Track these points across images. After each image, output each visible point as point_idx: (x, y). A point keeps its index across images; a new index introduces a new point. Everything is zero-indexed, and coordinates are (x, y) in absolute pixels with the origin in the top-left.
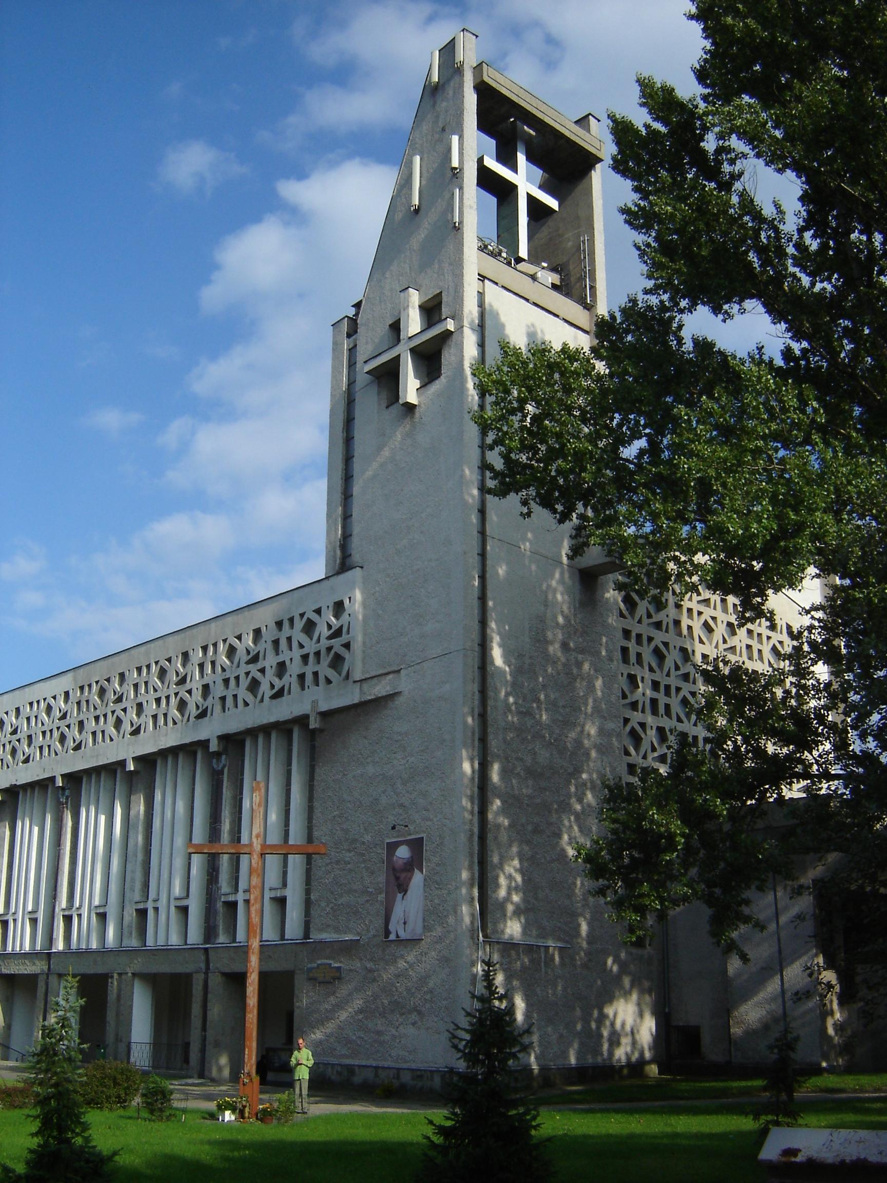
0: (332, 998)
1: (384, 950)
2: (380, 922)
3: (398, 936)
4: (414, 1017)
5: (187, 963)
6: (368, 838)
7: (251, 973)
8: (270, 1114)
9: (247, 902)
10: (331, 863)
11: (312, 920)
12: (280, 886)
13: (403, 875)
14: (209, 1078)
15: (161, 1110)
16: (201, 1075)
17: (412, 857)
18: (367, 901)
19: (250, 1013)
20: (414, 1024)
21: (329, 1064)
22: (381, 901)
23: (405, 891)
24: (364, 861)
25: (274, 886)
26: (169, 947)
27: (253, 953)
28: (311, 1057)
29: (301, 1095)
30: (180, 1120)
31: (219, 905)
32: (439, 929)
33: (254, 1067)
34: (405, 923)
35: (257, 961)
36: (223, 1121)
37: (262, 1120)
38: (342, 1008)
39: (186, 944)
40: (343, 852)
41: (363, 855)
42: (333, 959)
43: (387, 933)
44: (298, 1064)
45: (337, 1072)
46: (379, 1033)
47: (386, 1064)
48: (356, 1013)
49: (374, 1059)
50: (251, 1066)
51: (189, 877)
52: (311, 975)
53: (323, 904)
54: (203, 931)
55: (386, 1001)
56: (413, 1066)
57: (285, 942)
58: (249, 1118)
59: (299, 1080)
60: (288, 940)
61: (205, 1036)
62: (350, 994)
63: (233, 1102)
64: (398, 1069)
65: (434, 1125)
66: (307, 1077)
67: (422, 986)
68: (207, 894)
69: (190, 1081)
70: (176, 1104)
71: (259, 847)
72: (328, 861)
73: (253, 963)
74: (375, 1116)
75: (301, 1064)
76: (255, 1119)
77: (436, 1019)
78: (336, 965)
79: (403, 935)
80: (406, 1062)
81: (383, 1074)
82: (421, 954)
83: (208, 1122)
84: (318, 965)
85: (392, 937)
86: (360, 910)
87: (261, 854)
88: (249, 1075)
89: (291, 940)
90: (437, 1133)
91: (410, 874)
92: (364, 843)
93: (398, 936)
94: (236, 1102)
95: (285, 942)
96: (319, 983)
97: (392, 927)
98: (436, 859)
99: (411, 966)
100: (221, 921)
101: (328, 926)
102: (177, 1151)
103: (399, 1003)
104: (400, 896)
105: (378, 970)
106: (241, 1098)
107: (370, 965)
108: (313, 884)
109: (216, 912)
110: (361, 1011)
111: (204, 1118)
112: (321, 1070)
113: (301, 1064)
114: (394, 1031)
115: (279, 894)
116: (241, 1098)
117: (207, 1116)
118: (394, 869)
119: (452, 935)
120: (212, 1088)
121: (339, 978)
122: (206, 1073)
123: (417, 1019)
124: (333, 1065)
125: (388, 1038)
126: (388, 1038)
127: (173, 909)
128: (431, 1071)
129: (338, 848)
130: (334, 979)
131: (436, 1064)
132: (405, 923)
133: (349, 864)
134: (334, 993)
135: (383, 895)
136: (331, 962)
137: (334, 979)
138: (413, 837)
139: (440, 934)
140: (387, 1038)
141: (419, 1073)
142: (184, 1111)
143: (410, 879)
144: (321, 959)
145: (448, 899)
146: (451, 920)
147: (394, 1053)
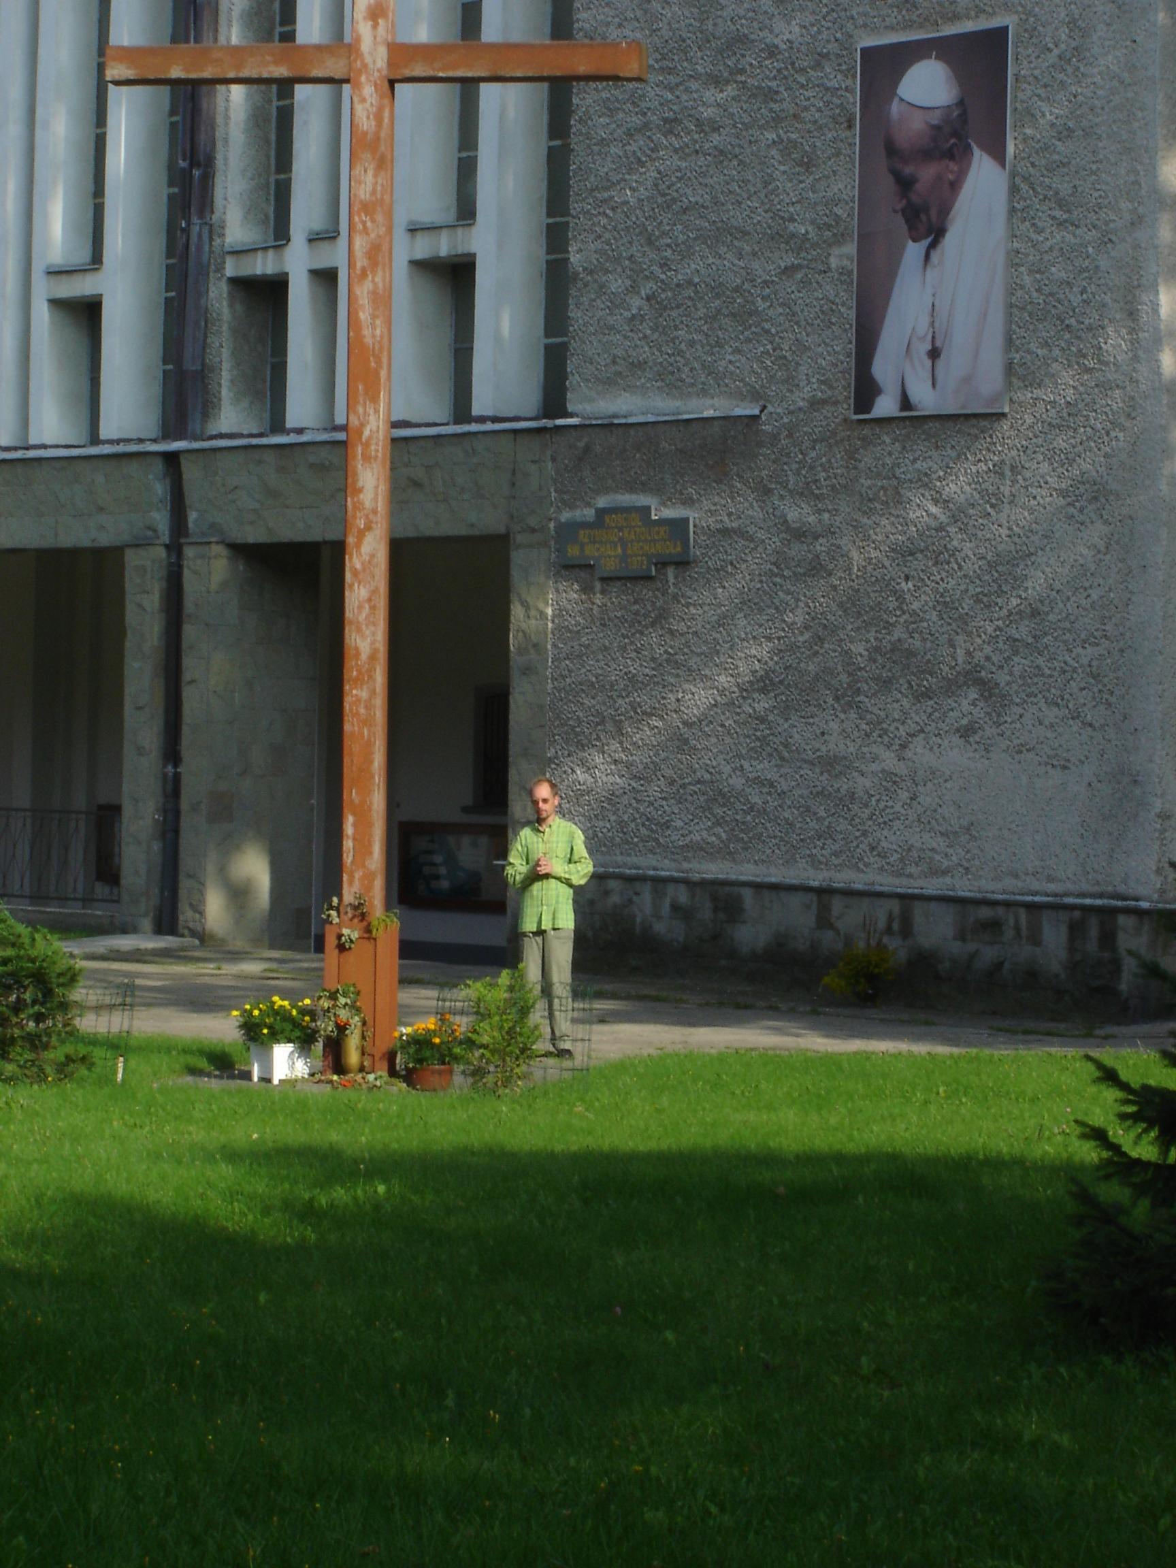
0: (654, 637)
1: (851, 455)
2: (843, 344)
3: (906, 403)
4: (967, 704)
5: (101, 509)
6: (788, 31)
7: (361, 534)
8: (446, 1056)
9: (326, 278)
10: (646, 126)
11: (573, 344)
12: (450, 217)
13: (926, 174)
14: (193, 934)
15: (35, 1042)
16: (166, 923)
17: (961, 103)
18: (788, 271)
19: (358, 681)
20: (966, 732)
21: (643, 879)
22: (843, 271)
23: (936, 233)
24: (777, 120)
25: (427, 218)
26: (31, 454)
27: (367, 458)
28: (581, 850)
29: (547, 991)
30: (107, 1080)
31: (218, 297)
32: (1067, 377)
33: (379, 885)
34: (934, 354)
35: (383, 488)
36: (267, 1080)
37: (409, 1078)
38: (693, 674)
39: (95, 439)
40: (694, 85)
41: (770, 95)
42: (658, 490)
43: (866, 391)
44: (536, 876)
45: (675, 907)
46: (830, 764)
47: (858, 881)
48: (746, 691)
49: (815, 862)
50: (369, 877)
51: (98, 190)
52: (573, 551)
53: (616, 284)
54: (157, 390)
55: (859, 648)
56: (964, 887)
57: (474, 427)
58: (362, 1069)
59: (540, 933)
60: (482, 419)
61: (177, 778)
62: (722, 622)
63: (304, 1011)
64: (906, 899)
65: (1124, 1086)
66: (567, 920)
67: (1000, 592)
68: (170, 251)
69: (125, 943)
70: (88, 1023)
71: (382, 52)
72: (637, 121)
73: (367, 498)
74: (831, 1063)
75: (547, 876)
76: (384, 1073)
77: (1051, 714)
78: (669, 513)
79: (926, 398)
80: (936, 872)
81: (848, 918)
82: (998, 470)
83: (214, 1085)
84: (601, 513)
85: (885, 406)
86: (761, 305)
87: (392, 83)
88: (360, 912)
89: (495, 420)
90: (1135, 1118)
91: (953, 166)
92: (772, 51)
93: (906, 403)
94: (312, 1013)
95: (474, 427)
96: (605, 580)
97: (883, 369)
98: (1050, 113)
99: (958, 515)
100: (225, 353)
101: (639, 365)
102: (119, 1185)
103: (910, 653)
104: (913, 251)
105: (830, 532)
106: (333, 996)
107: (798, 513)
108: (575, 207)
109: (206, 319)
110: (764, 683)
111: (193, 1071)
112: (615, 899)
113: (547, 876)
114: (889, 759)
115: (444, 246)
116: (333, 996)
117: (203, 1064)
118: (891, 149)
119: (1117, 400)
120: (209, 968)
121: (683, 563)
122: (186, 915)
123: (978, 713)
124: (660, 883)
125: (867, 782)
126: (867, 782)
127: (42, 313)
128: (1031, 907)
129: (670, 71)
130: (662, 564)
131: (1050, 879)
132: (934, 354)
133: (716, 129)
134: (662, 616)
135: (851, 248)
136: (641, 500)
137: (662, 564)
138: (968, 26)
139: (1070, 395)
140: (863, 784)
141: (985, 913)
142: (118, 1046)
143: (955, 186)
144: (607, 490)
145: (1104, 263)
146: (1115, 342)
147: (889, 839)
